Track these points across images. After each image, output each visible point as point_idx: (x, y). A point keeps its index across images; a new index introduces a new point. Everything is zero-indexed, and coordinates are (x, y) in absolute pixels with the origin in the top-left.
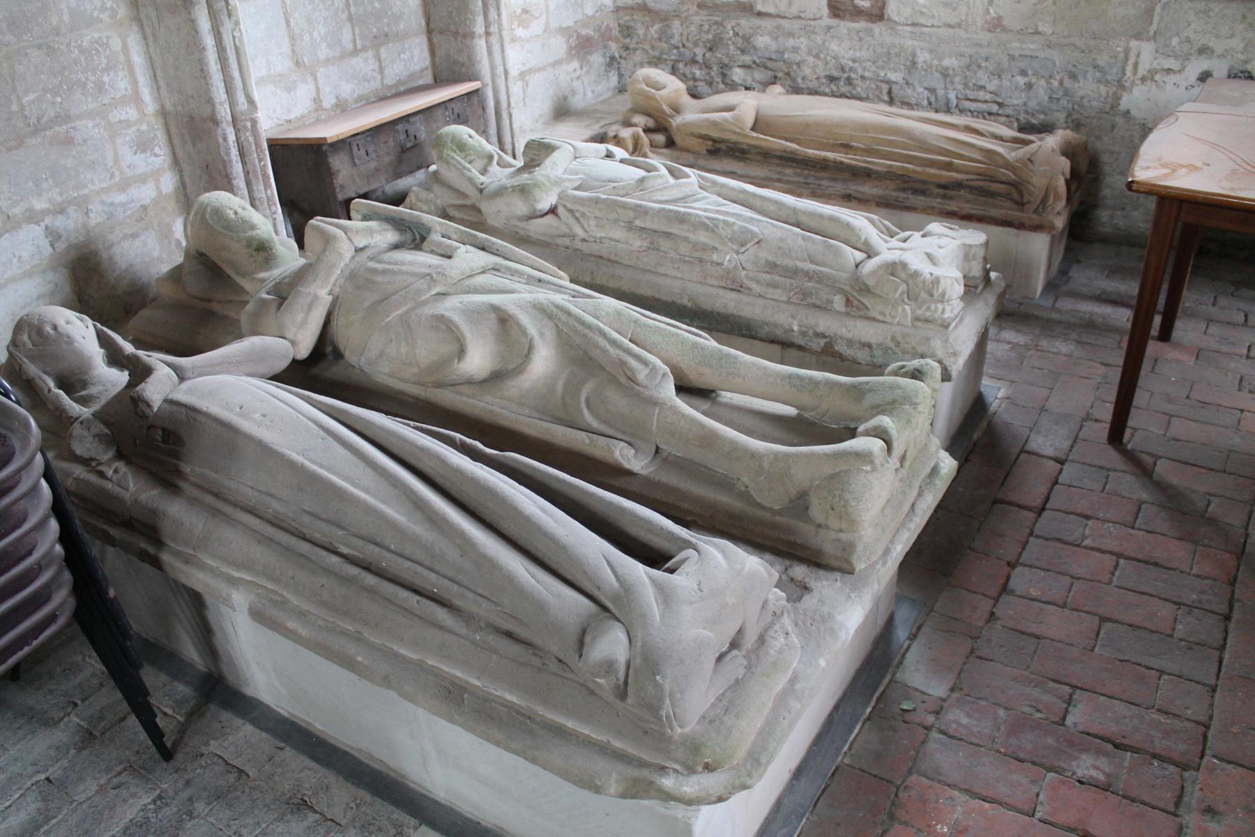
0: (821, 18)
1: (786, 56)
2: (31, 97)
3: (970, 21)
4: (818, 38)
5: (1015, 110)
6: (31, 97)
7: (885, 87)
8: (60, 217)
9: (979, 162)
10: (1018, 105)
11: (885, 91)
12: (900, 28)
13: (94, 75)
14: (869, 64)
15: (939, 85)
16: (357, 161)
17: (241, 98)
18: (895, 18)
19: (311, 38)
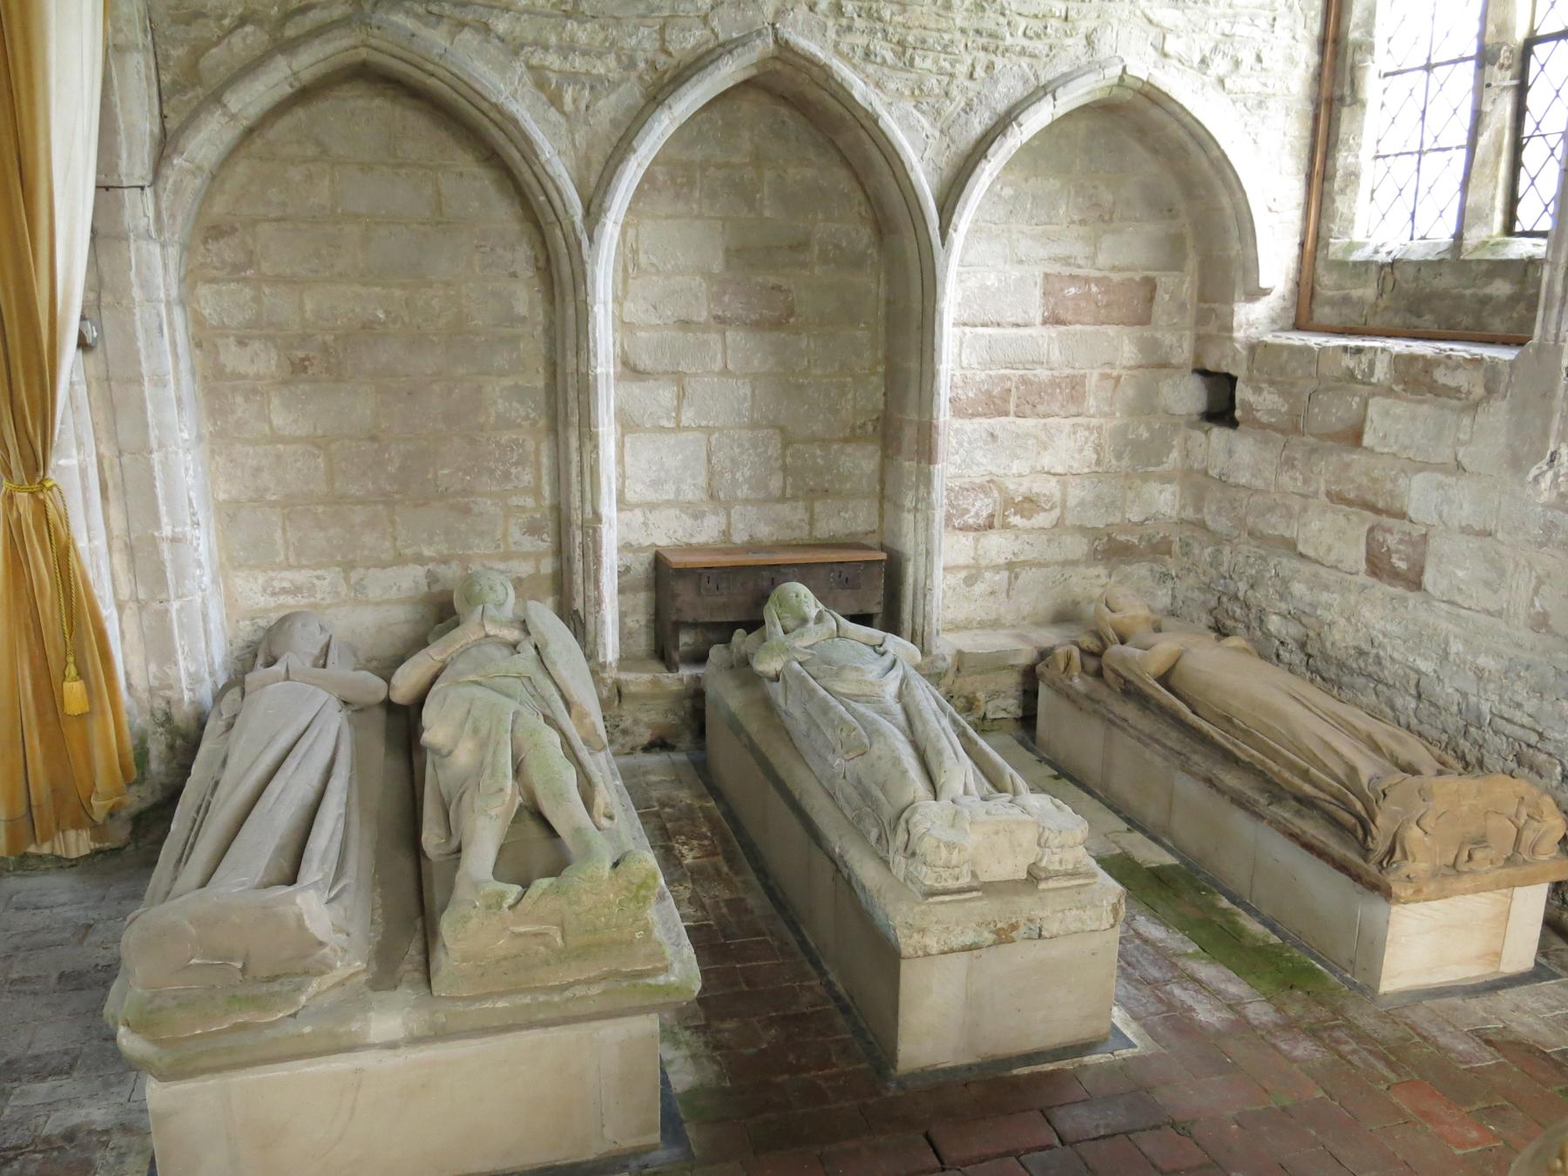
0: (1357, 573)
1: (1319, 612)
2: (445, 472)
3: (1512, 611)
4: (1352, 597)
5: (1556, 747)
6: (445, 472)
7: (1413, 677)
8: (443, 566)
9: (1337, 779)
10: (1561, 742)
11: (1413, 683)
12: (1436, 603)
13: (504, 465)
14: (1399, 641)
15: (1471, 689)
16: (703, 592)
17: (588, 508)
18: (1430, 588)
19: (733, 477)
